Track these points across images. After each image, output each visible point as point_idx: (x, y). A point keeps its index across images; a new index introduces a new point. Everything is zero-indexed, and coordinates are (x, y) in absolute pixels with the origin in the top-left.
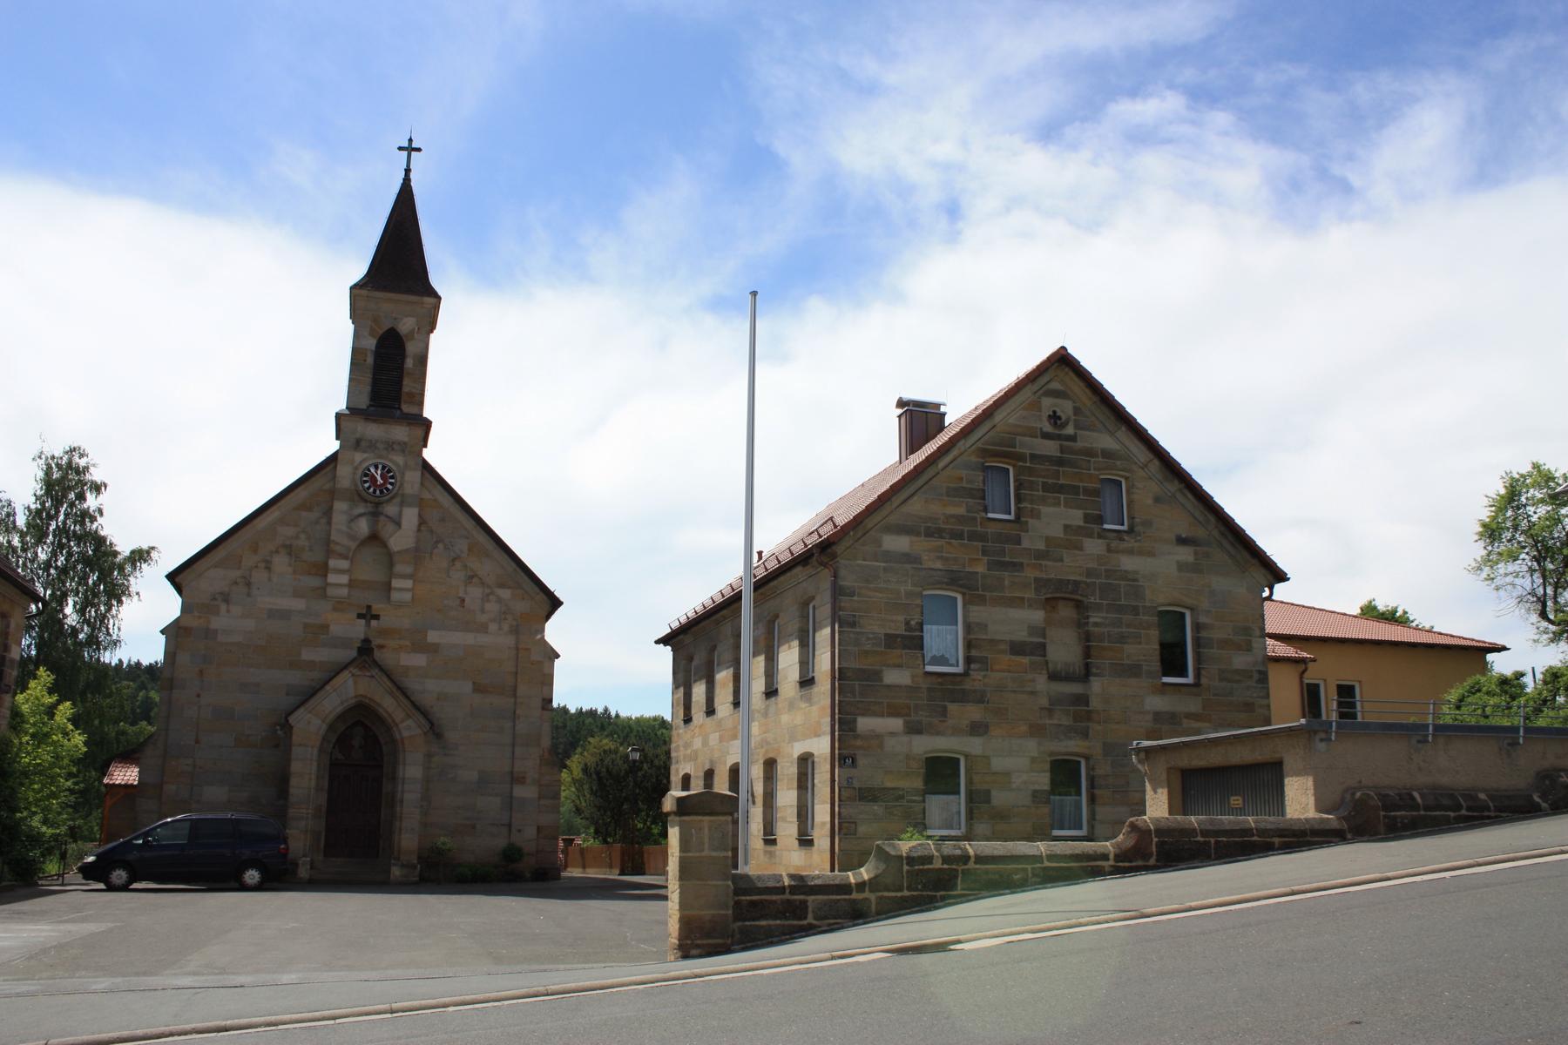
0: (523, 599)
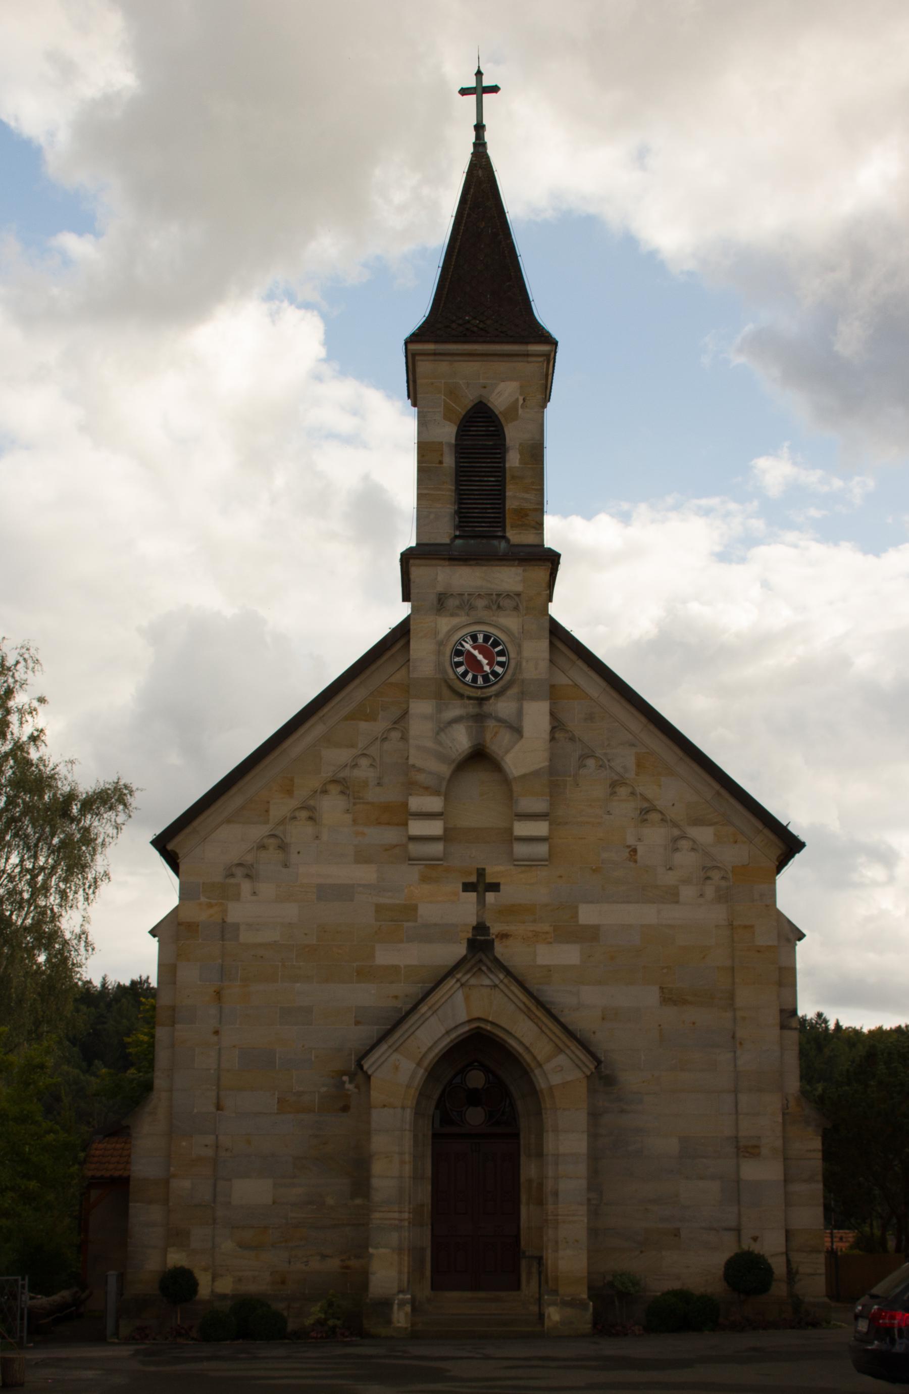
0: (736, 842)
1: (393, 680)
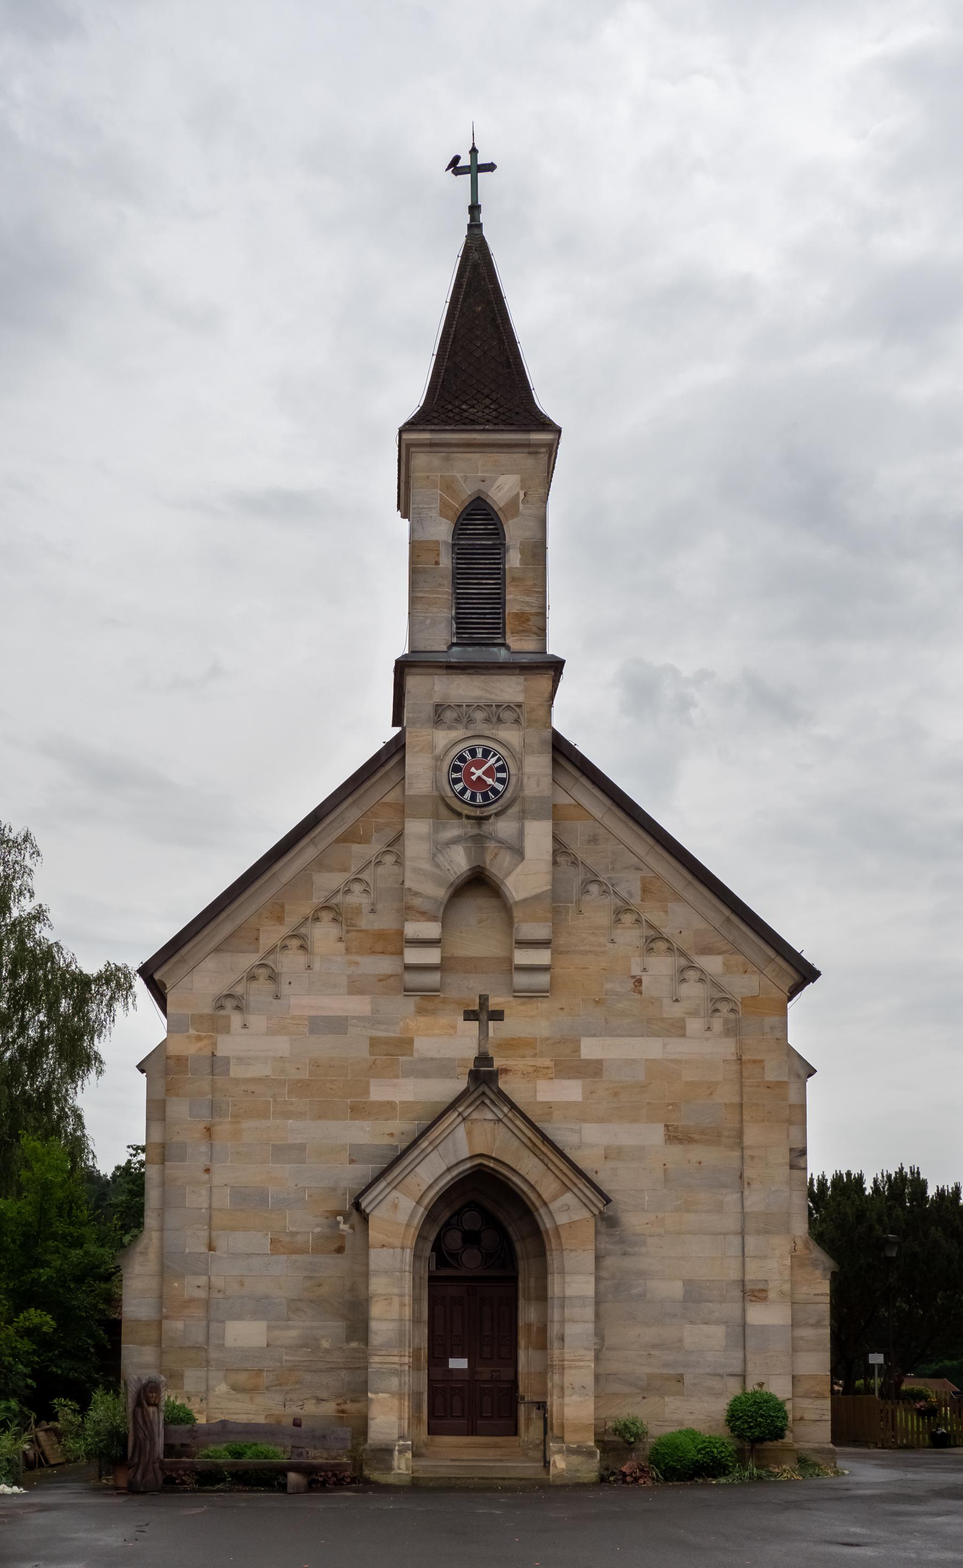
0: (746, 972)
1: (387, 799)
